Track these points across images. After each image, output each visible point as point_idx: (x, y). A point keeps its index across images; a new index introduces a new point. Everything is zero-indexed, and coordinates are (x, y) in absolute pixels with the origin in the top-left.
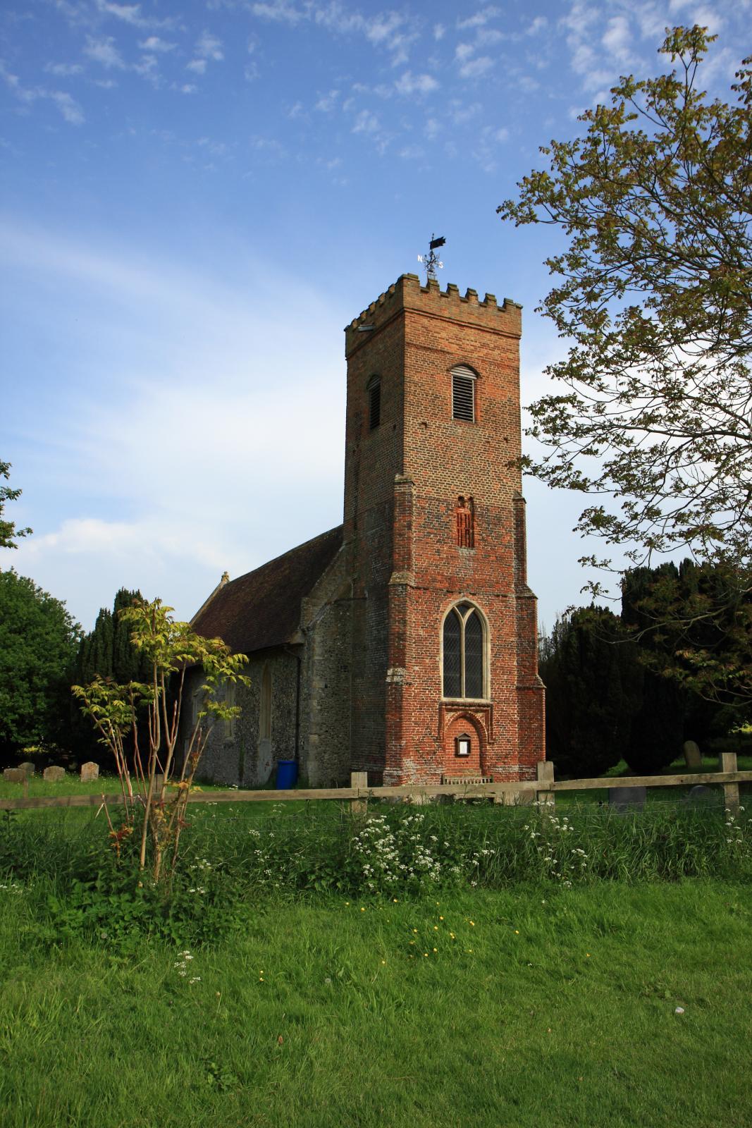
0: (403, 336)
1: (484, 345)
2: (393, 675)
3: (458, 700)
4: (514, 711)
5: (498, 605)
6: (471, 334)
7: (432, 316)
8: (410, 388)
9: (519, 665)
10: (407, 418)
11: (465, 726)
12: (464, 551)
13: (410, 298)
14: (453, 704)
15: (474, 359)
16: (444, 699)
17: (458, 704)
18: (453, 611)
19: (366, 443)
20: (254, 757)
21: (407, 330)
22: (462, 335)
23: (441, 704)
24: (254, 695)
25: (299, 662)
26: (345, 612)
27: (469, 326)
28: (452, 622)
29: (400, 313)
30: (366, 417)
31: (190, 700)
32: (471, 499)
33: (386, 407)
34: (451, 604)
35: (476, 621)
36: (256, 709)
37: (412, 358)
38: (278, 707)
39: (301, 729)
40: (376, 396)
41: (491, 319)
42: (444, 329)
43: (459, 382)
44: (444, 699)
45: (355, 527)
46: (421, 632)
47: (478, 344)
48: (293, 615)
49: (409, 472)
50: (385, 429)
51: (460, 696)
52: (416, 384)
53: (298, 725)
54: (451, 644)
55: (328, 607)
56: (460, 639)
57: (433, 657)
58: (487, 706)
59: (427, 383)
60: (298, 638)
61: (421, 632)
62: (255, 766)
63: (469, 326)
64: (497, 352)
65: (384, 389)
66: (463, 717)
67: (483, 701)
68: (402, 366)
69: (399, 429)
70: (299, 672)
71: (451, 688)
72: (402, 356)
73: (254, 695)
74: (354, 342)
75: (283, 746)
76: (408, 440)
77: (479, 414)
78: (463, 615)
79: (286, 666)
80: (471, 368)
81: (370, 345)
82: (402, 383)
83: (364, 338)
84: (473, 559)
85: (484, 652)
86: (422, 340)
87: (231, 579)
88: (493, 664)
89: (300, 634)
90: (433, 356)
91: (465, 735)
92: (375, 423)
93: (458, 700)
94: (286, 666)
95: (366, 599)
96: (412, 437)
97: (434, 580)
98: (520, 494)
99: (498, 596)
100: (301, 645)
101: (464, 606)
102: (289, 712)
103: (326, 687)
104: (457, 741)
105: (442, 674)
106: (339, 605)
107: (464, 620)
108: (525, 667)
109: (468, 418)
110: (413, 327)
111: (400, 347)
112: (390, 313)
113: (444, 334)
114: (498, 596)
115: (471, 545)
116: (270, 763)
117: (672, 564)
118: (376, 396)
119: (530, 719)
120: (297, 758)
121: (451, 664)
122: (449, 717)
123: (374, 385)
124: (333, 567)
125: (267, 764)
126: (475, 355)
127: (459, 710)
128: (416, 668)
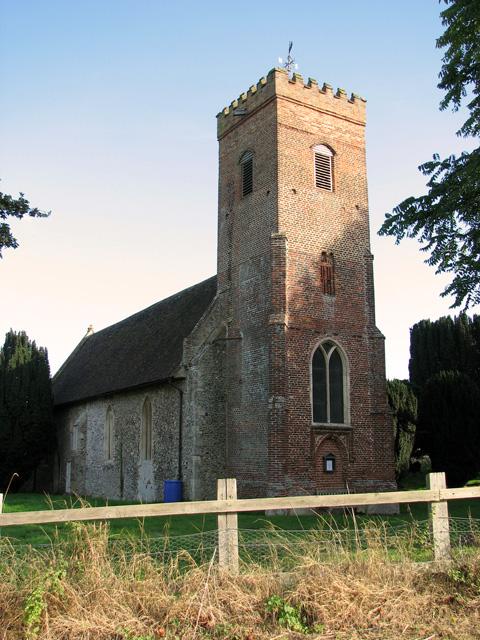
0: (276, 118)
1: (338, 129)
2: (274, 403)
3: (325, 424)
4: (369, 434)
5: (354, 345)
6: (328, 120)
7: (298, 103)
8: (282, 160)
9: (374, 395)
10: (280, 185)
11: (329, 448)
12: (327, 298)
13: (281, 87)
14: (321, 428)
15: (331, 139)
16: (314, 424)
17: (325, 428)
18: (319, 349)
19: (239, 207)
20: (135, 475)
21: (279, 112)
22: (321, 120)
23: (313, 428)
24: (134, 424)
25: (181, 393)
26: (221, 350)
27: (326, 113)
28: (319, 358)
29: (272, 99)
30: (238, 185)
31: (68, 430)
32: (332, 254)
33: (258, 177)
34: (319, 343)
35: (336, 356)
36: (137, 436)
37: (283, 135)
38: (160, 434)
39: (183, 452)
40: (248, 170)
41: (342, 107)
42: (307, 114)
43: (319, 157)
44: (314, 424)
45: (230, 279)
46: (295, 366)
47: (333, 128)
48: (174, 352)
49: (282, 230)
50: (255, 197)
51: (326, 421)
52: (286, 157)
53: (181, 449)
54: (319, 377)
55: (207, 346)
56: (325, 372)
57: (305, 388)
58: (348, 429)
59: (294, 158)
60: (181, 373)
61: (295, 366)
62: (135, 484)
63: (326, 113)
64: (348, 135)
65: (256, 163)
66: (329, 439)
67: (344, 425)
68: (275, 142)
69: (272, 193)
70: (181, 403)
71: (319, 416)
72: (275, 134)
73: (134, 424)
74: (226, 125)
75: (165, 466)
76: (282, 202)
77: (336, 184)
78: (327, 352)
79: (167, 398)
80: (329, 147)
81: (242, 127)
82: (276, 156)
83: (236, 121)
84: (336, 304)
85: (344, 384)
86: (290, 122)
87: (96, 331)
88: (351, 394)
89: (183, 369)
90: (299, 135)
91: (331, 454)
92: (248, 189)
93: (325, 424)
94: (167, 398)
95: (241, 339)
96: (285, 200)
97: (304, 322)
98: (369, 251)
99: (354, 336)
100: (184, 379)
101: (328, 345)
102: (171, 437)
103: (207, 414)
104: (325, 460)
105: (311, 402)
106: (217, 345)
107: (328, 357)
108: (378, 396)
109: (327, 187)
110: (283, 111)
111: (273, 126)
112: (262, 100)
113: (307, 118)
114: (354, 336)
115: (332, 293)
116: (152, 482)
117: (449, 317)
118: (248, 170)
119: (383, 440)
120: (180, 476)
121: (319, 393)
122: (318, 439)
123: (246, 159)
124: (210, 312)
125: (149, 483)
126: (332, 137)
127: (325, 433)
128: (292, 397)
